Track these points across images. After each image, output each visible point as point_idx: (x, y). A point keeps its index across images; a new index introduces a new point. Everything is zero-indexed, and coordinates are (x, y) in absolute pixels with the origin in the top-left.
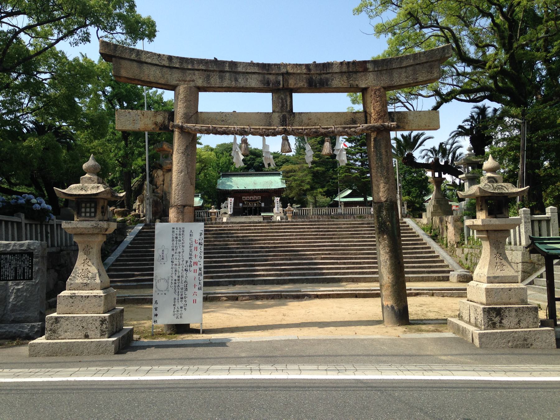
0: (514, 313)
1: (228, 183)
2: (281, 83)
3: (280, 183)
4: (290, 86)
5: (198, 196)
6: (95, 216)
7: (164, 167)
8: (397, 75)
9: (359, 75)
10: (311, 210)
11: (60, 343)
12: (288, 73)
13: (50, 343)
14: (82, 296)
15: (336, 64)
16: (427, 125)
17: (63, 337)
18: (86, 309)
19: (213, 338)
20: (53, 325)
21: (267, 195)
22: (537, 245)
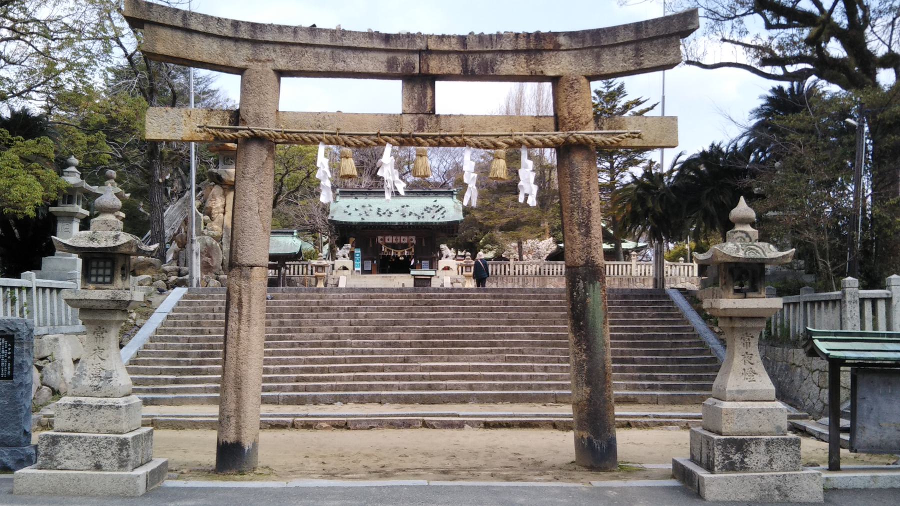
0: (763, 448)
2: (417, 65)
4: (430, 72)
6: (111, 282)
8: (608, 57)
9: (546, 55)
11: (61, 475)
12: (428, 51)
13: (45, 474)
14: (91, 406)
15: (508, 37)
16: (658, 140)
17: (63, 466)
18: (97, 427)
22: (817, 342)
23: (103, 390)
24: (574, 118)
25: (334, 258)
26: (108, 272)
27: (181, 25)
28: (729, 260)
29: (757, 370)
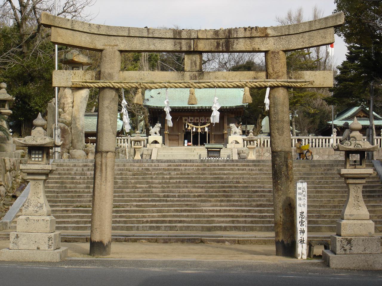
19: (305, 209)
20: (15, 240)
23: (39, 212)
24: (276, 73)
25: (148, 134)
26: (40, 156)
27: (70, 28)
28: (348, 150)
29: (360, 205)
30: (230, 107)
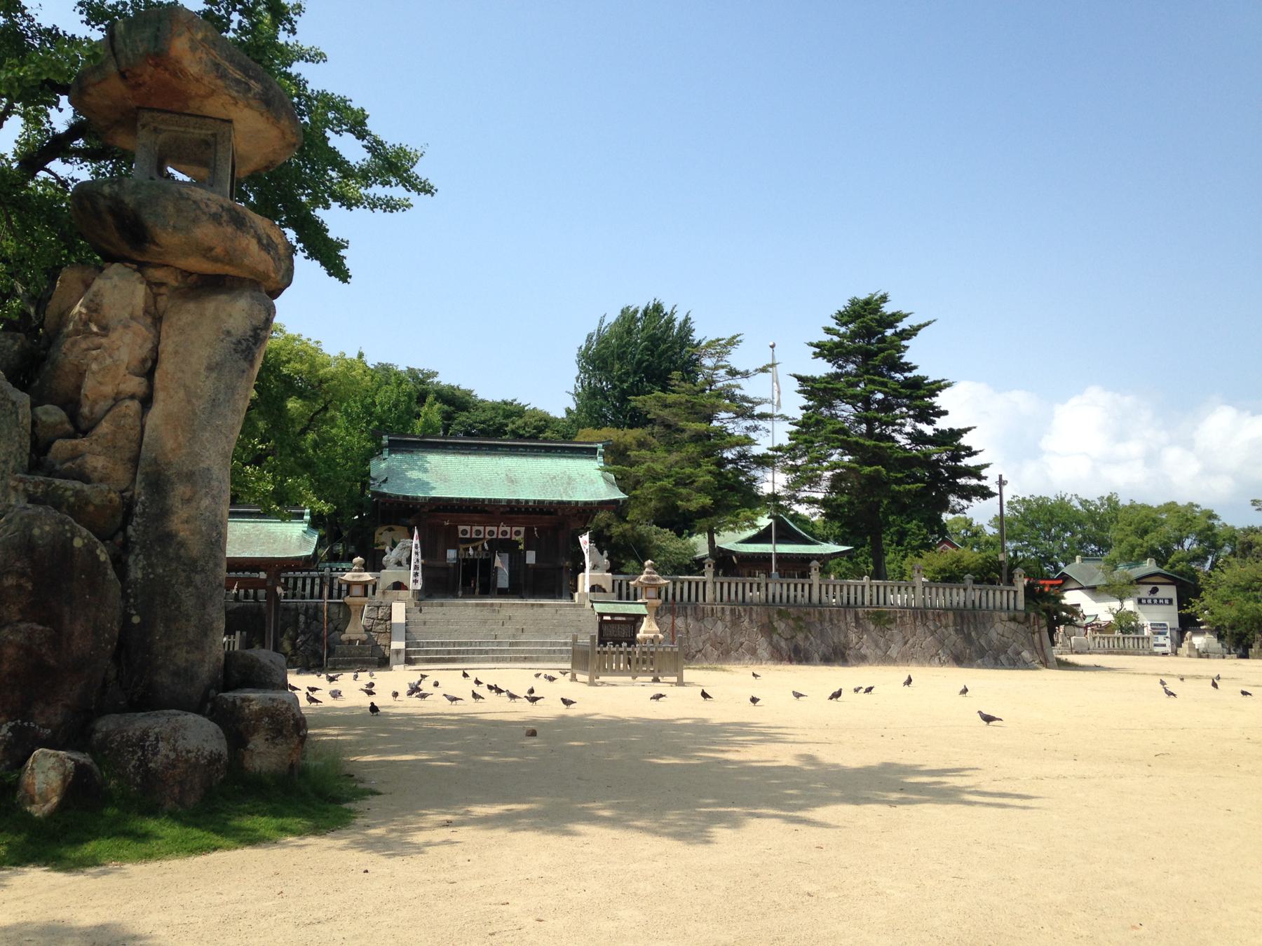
1: (414, 474)
3: (601, 482)
5: (301, 516)
7: (167, 238)
10: (709, 586)
21: (554, 524)
30: (586, 503)
